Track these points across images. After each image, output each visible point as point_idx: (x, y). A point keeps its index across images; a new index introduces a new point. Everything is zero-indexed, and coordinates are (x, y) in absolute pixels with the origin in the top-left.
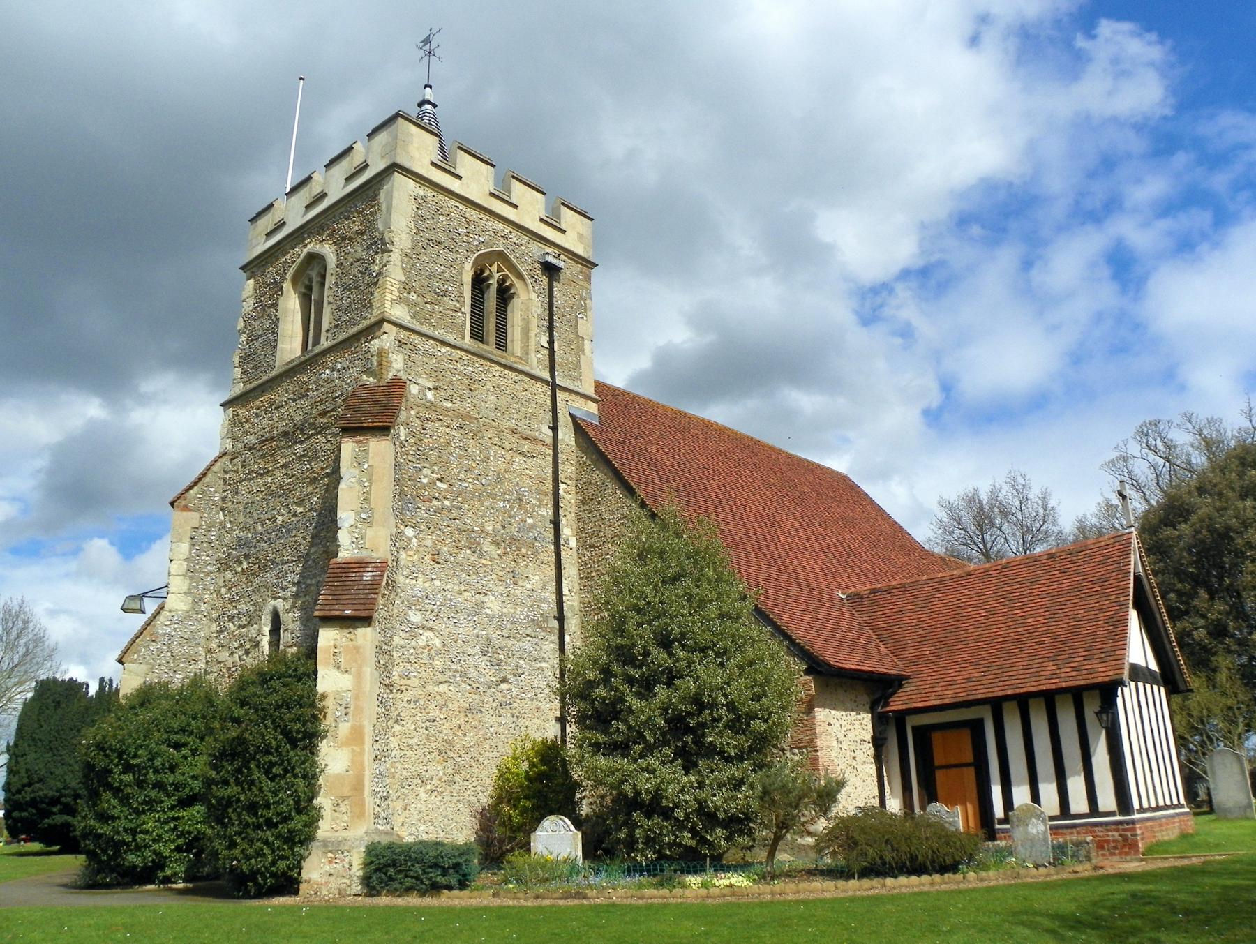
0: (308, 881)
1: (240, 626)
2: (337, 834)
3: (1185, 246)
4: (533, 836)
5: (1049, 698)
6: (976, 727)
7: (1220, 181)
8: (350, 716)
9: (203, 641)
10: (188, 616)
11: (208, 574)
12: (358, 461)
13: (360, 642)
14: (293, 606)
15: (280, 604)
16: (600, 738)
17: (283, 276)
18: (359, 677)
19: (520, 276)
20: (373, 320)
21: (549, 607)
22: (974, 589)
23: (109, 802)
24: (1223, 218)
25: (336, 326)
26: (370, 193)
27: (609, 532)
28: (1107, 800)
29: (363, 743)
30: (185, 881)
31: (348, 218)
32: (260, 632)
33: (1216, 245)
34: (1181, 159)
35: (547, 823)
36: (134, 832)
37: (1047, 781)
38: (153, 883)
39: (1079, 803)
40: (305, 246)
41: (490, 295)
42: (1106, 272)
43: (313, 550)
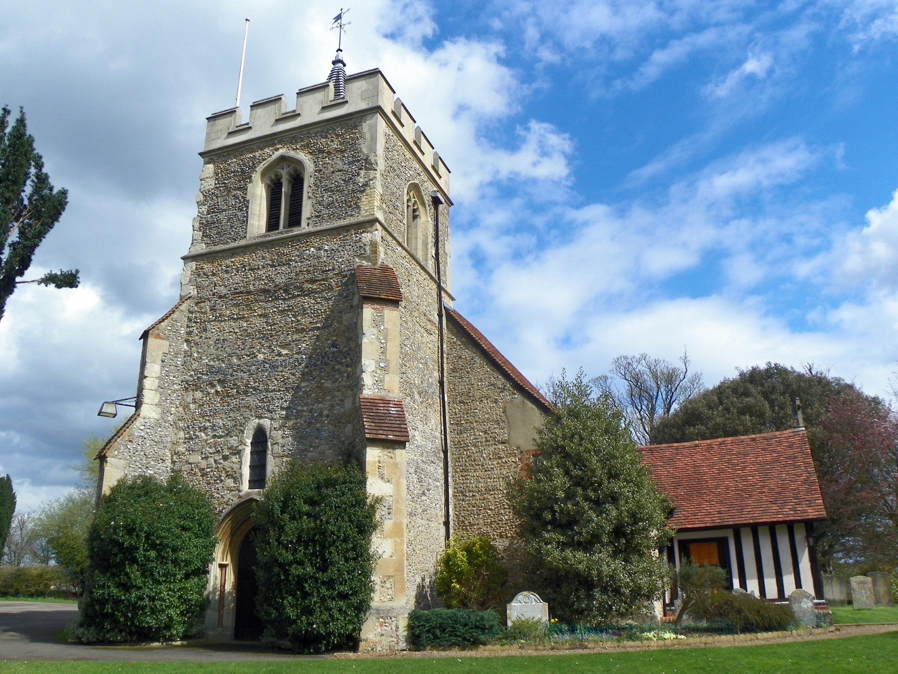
0: (366, 640)
1: (214, 436)
2: (385, 604)
3: (517, 256)
4: (508, 606)
5: (772, 527)
6: (722, 543)
7: (539, 221)
8: (392, 515)
9: (169, 445)
11: (174, 391)
12: (377, 324)
13: (398, 459)
14: (282, 426)
16: (562, 538)
17: (253, 168)
18: (398, 486)
19: (423, 204)
20: (361, 219)
22: (704, 455)
23: (134, 573)
24: (542, 245)
25: (317, 217)
26: (350, 123)
27: (478, 394)
29: (403, 536)
30: (182, 639)
31: (326, 137)
32: (242, 443)
33: (537, 258)
34: (517, 202)
35: (520, 597)
36: (152, 599)
37: (770, 577)
38: (159, 641)
39: (771, 590)
40: (277, 150)
42: (468, 262)
43: (303, 384)
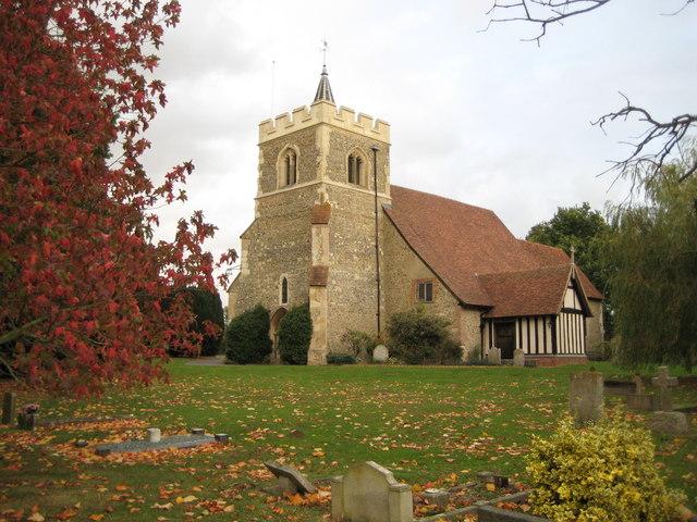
5: (536, 318)
10: (248, 276)
15: (286, 275)
21: (375, 312)
28: (549, 350)
41: (354, 165)
